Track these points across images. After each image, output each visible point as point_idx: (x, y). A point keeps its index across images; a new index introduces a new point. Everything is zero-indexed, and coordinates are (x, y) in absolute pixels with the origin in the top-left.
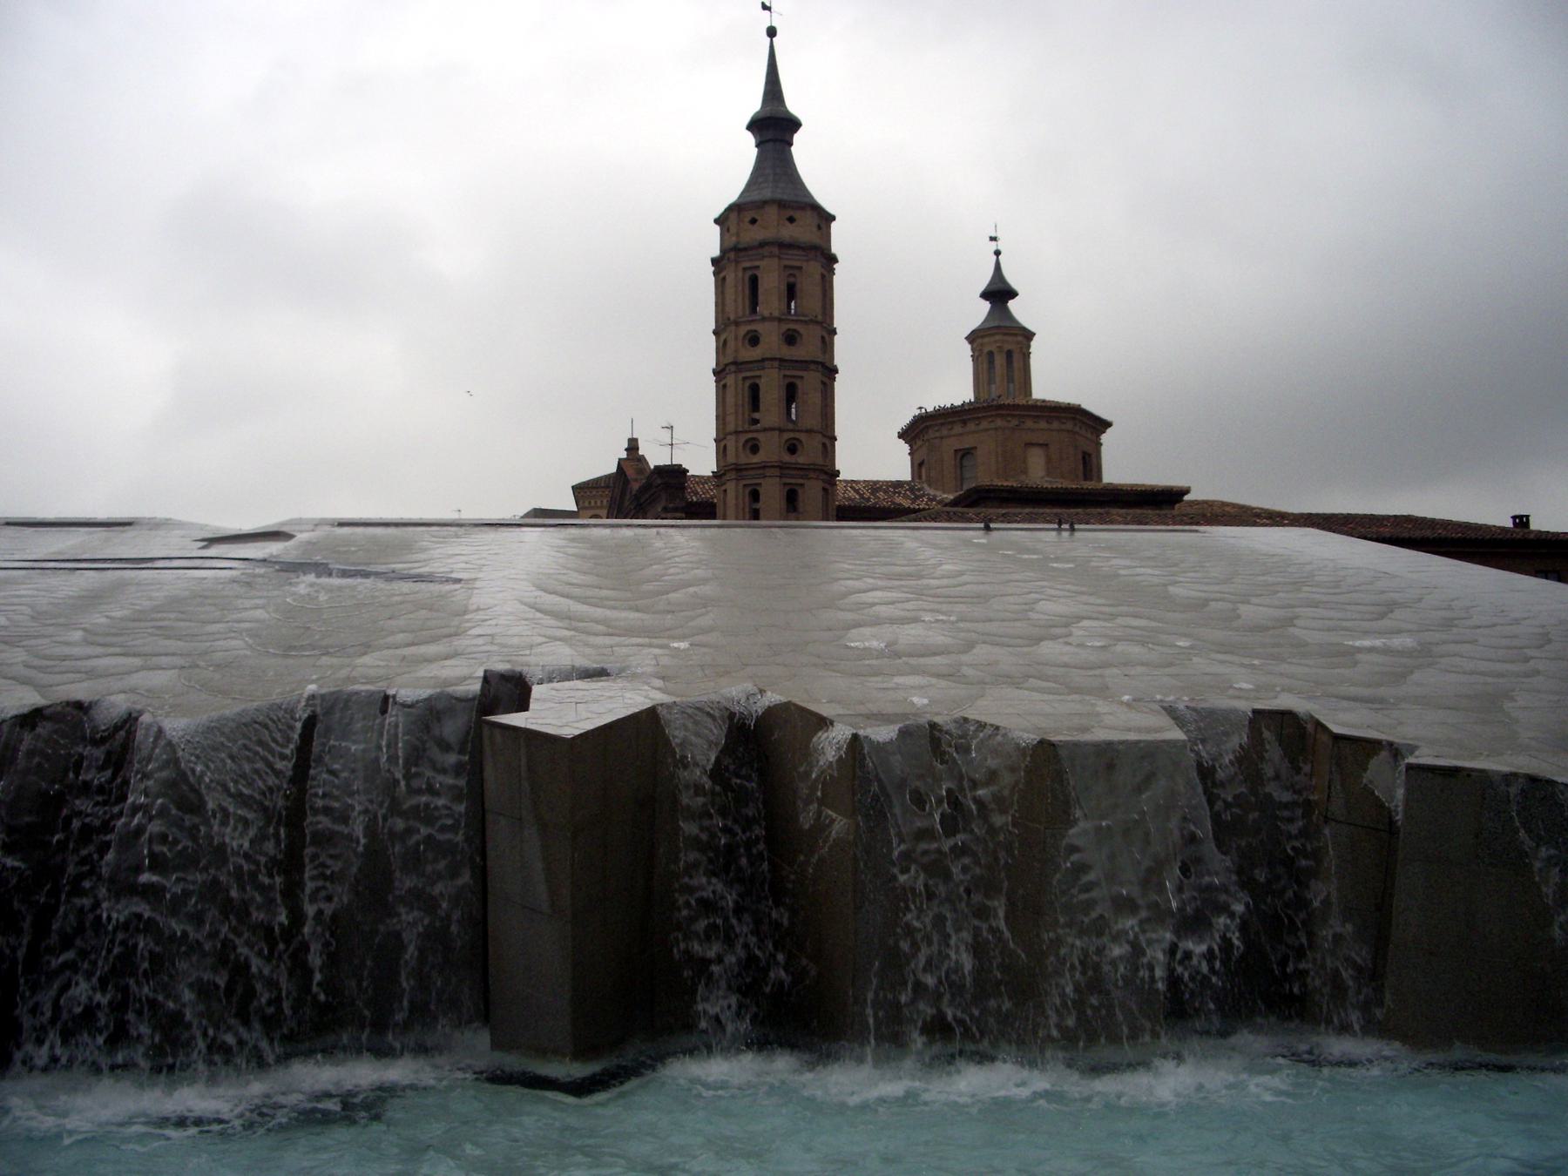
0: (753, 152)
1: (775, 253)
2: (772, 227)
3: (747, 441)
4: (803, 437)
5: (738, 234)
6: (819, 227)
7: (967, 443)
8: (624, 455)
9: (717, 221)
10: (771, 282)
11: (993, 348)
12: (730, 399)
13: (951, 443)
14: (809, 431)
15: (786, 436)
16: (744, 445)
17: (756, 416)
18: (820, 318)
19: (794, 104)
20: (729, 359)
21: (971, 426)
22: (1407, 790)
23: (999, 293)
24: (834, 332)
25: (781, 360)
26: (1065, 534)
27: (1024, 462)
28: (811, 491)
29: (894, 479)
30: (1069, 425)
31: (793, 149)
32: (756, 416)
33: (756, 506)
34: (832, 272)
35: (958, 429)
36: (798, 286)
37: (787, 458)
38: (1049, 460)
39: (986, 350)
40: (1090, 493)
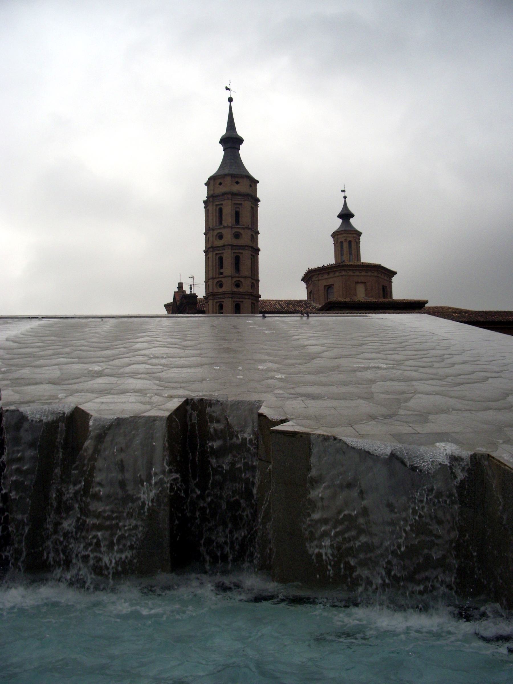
0: (222, 153)
1: (232, 199)
2: (229, 186)
3: (218, 282)
4: (242, 280)
5: (214, 190)
6: (251, 186)
7: (330, 282)
8: (177, 290)
9: (206, 184)
10: (228, 210)
11: (343, 240)
12: (210, 264)
14: (245, 277)
15: (235, 279)
16: (216, 284)
17: (221, 271)
18: (250, 226)
19: (240, 132)
20: (210, 246)
21: (331, 275)
22: (88, 424)
23: (346, 215)
24: (258, 233)
25: (232, 246)
26: (305, 318)
27: (356, 290)
28: (247, 303)
29: (298, 299)
30: (376, 274)
31: (240, 151)
32: (221, 271)
34: (257, 206)
35: (326, 276)
36: (240, 213)
37: (236, 290)
38: (366, 290)
39: (340, 241)
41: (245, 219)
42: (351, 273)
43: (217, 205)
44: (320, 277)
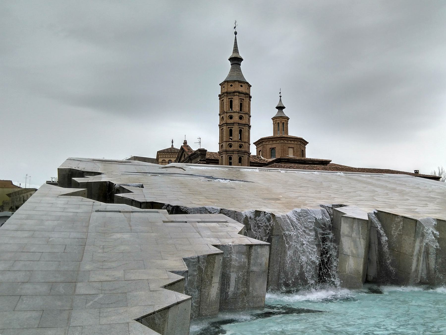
4: (243, 144)
10: (236, 103)
13: (269, 146)
14: (245, 142)
17: (231, 137)
24: (250, 116)
30: (299, 143)
33: (231, 161)
35: (271, 143)
37: (239, 149)
38: (294, 152)
39: (277, 122)
40: (302, 160)
41: (245, 109)
42: (286, 142)
43: (229, 98)
44: (267, 143)
